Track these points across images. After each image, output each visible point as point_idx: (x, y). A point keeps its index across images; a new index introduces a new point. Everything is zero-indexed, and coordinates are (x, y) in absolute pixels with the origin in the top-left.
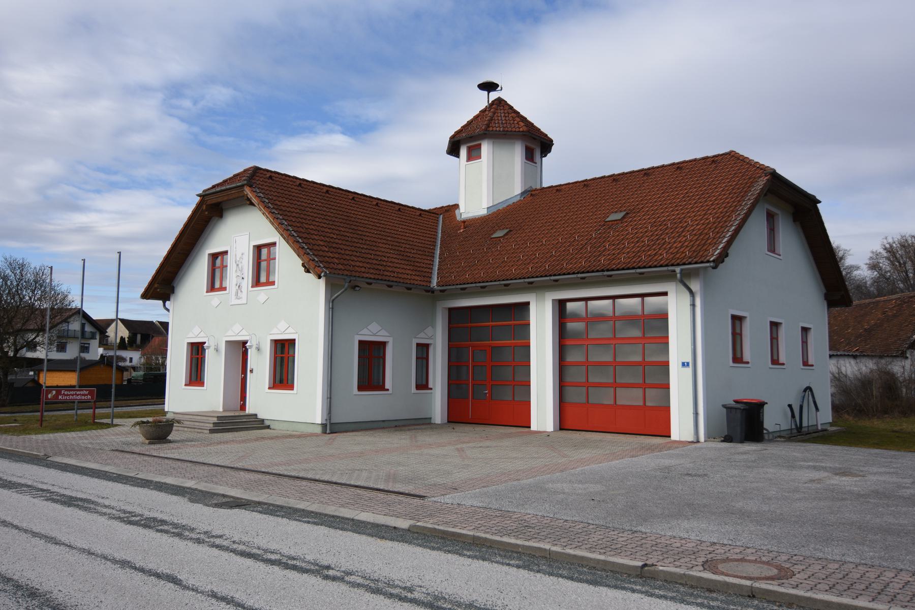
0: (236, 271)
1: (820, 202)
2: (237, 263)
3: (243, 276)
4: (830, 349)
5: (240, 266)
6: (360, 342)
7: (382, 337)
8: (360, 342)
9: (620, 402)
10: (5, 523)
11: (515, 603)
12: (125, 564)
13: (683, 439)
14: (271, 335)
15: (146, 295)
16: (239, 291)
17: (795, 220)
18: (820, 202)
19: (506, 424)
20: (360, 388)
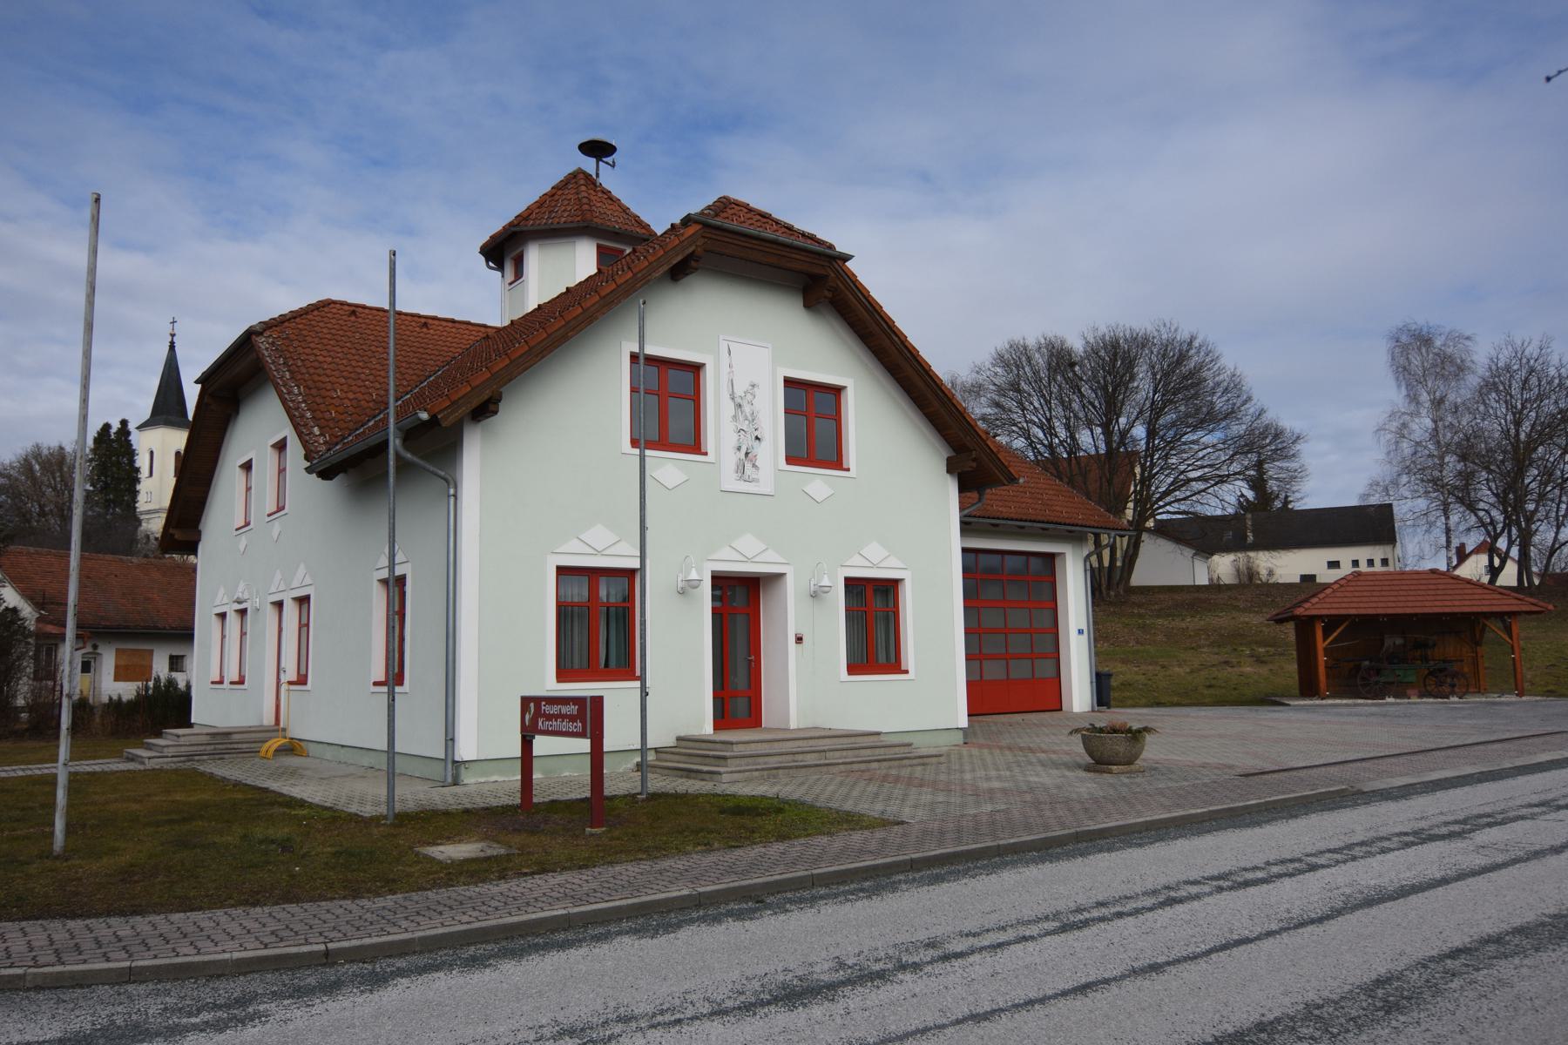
0: (735, 417)
1: (847, 258)
2: (738, 400)
3: (756, 433)
4: (194, 569)
5: (747, 409)
6: (847, 580)
7: (766, 565)
8: (847, 580)
9: (1013, 675)
10: (1557, 850)
11: (855, 938)
12: (1404, 892)
13: (801, 727)
14: (709, 562)
15: (251, 460)
16: (748, 466)
17: (809, 305)
18: (847, 258)
19: (1045, 708)
20: (853, 669)
